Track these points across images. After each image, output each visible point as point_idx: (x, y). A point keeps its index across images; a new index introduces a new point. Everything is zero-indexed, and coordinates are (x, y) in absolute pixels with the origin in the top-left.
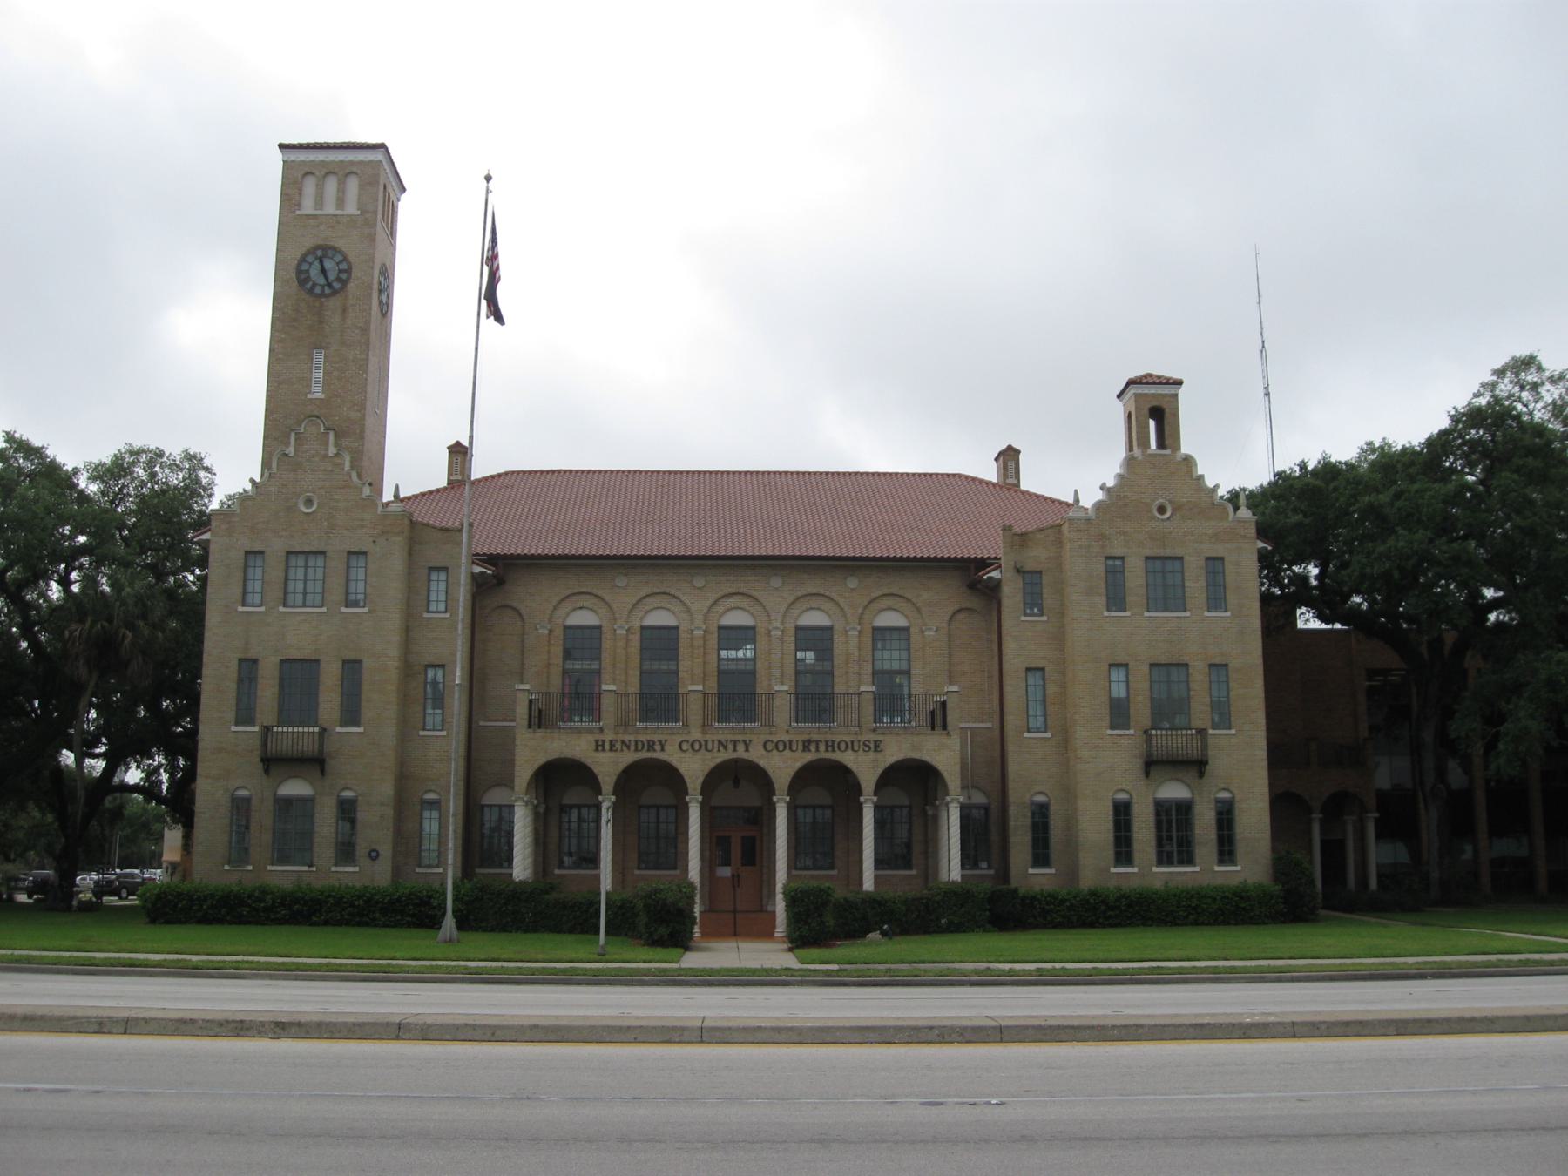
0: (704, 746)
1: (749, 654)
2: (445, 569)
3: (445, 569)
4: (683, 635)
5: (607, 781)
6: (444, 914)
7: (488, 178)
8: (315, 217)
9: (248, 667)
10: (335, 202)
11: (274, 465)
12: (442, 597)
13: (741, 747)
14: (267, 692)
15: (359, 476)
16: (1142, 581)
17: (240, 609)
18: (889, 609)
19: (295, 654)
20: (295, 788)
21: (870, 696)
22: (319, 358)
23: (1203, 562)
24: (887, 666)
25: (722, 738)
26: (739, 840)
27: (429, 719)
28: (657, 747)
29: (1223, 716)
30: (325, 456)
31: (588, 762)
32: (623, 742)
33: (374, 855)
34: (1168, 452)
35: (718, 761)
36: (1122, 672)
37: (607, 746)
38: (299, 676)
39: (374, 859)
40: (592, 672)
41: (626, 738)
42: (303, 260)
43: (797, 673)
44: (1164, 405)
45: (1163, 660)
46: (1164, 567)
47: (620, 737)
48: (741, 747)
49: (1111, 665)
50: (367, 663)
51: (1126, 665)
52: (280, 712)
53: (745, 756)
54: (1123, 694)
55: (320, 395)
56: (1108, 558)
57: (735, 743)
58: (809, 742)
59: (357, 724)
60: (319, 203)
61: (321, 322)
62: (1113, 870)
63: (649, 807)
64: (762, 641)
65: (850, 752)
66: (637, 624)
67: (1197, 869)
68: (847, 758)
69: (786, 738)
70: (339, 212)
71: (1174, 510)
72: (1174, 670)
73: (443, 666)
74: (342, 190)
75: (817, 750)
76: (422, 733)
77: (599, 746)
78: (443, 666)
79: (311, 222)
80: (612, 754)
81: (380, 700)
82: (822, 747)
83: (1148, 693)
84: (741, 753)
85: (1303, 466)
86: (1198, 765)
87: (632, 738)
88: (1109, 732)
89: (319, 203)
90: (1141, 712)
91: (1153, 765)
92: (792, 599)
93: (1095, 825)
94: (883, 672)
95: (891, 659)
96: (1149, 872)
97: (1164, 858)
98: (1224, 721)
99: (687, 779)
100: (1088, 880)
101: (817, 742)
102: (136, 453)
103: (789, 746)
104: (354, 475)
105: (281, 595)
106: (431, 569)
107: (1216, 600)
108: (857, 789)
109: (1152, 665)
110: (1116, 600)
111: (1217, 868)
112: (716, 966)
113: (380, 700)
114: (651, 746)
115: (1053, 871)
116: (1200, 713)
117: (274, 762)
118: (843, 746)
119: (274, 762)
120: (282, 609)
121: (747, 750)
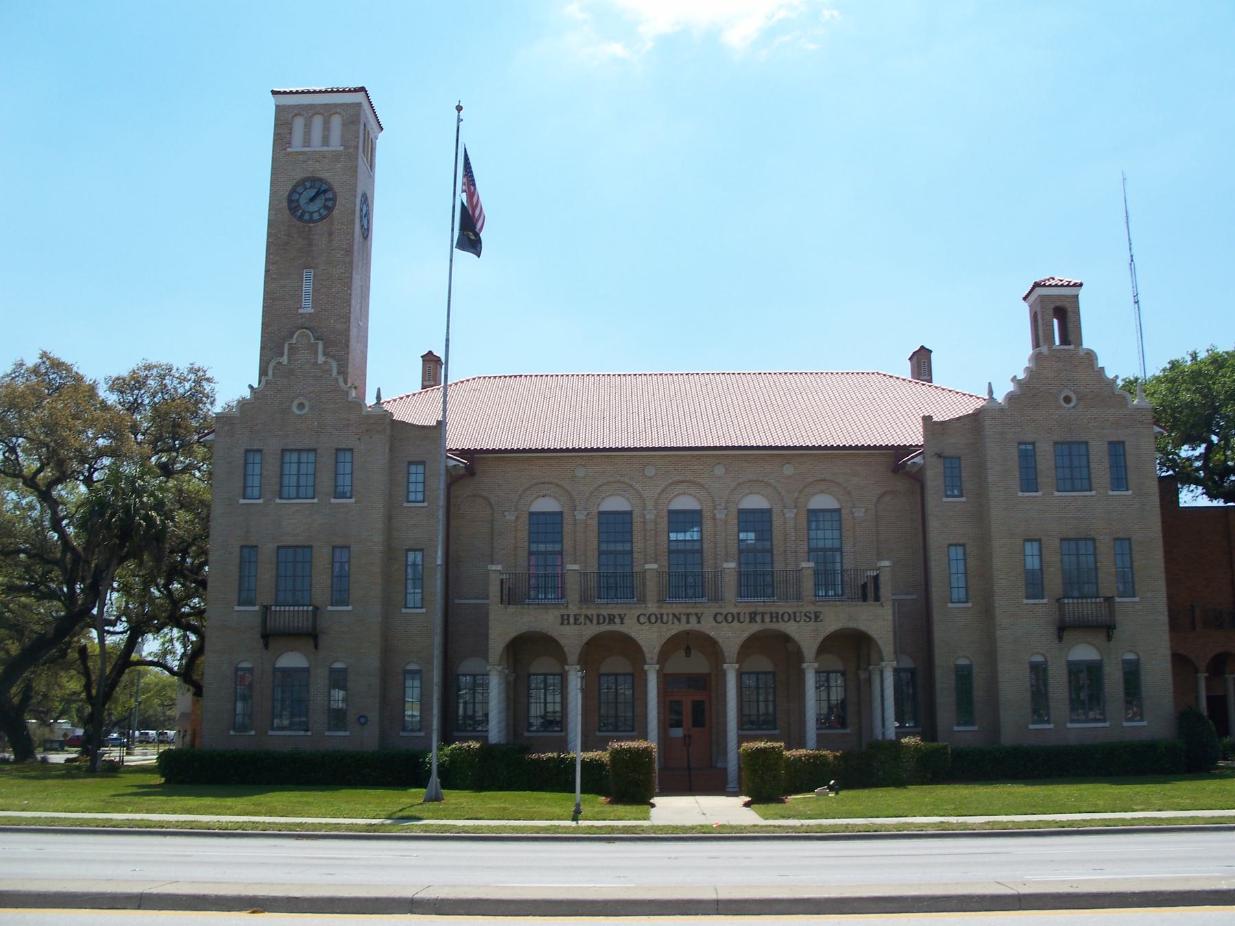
0: (660, 618)
2: (423, 463)
3: (423, 463)
4: (637, 520)
5: (809, 646)
7: (459, 108)
9: (249, 553)
11: (270, 372)
13: (693, 619)
14: (265, 575)
17: (242, 501)
18: (822, 492)
19: (290, 541)
20: (292, 660)
21: (810, 572)
22: (308, 276)
23: (1106, 447)
24: (821, 544)
25: (676, 611)
27: (410, 597)
28: (617, 620)
31: (555, 635)
32: (586, 616)
34: (1072, 347)
35: (674, 632)
36: (1036, 545)
37: (572, 620)
38: (295, 557)
41: (589, 613)
42: (293, 191)
44: (1052, 306)
46: (1072, 453)
47: (584, 612)
48: (693, 619)
51: (1039, 540)
53: (697, 627)
56: (1020, 443)
58: (755, 614)
60: (307, 141)
64: (708, 524)
65: (792, 622)
66: (595, 512)
68: (790, 628)
69: (735, 611)
70: (325, 149)
71: (1078, 399)
72: (1082, 544)
74: (327, 127)
75: (763, 621)
76: (404, 610)
77: (564, 620)
78: (422, 550)
79: (301, 158)
80: (576, 627)
82: (767, 619)
84: (693, 625)
85: (1194, 356)
87: (594, 612)
88: (1026, 601)
89: (307, 141)
90: (1054, 583)
91: (1063, 628)
93: (1013, 684)
95: (825, 537)
99: (645, 649)
100: (1009, 735)
101: (763, 614)
102: (149, 368)
103: (737, 617)
104: (341, 380)
106: (410, 463)
107: (1119, 480)
109: (1061, 540)
110: (1029, 482)
114: (611, 619)
115: (976, 728)
116: (1108, 583)
120: (278, 501)
121: (699, 622)
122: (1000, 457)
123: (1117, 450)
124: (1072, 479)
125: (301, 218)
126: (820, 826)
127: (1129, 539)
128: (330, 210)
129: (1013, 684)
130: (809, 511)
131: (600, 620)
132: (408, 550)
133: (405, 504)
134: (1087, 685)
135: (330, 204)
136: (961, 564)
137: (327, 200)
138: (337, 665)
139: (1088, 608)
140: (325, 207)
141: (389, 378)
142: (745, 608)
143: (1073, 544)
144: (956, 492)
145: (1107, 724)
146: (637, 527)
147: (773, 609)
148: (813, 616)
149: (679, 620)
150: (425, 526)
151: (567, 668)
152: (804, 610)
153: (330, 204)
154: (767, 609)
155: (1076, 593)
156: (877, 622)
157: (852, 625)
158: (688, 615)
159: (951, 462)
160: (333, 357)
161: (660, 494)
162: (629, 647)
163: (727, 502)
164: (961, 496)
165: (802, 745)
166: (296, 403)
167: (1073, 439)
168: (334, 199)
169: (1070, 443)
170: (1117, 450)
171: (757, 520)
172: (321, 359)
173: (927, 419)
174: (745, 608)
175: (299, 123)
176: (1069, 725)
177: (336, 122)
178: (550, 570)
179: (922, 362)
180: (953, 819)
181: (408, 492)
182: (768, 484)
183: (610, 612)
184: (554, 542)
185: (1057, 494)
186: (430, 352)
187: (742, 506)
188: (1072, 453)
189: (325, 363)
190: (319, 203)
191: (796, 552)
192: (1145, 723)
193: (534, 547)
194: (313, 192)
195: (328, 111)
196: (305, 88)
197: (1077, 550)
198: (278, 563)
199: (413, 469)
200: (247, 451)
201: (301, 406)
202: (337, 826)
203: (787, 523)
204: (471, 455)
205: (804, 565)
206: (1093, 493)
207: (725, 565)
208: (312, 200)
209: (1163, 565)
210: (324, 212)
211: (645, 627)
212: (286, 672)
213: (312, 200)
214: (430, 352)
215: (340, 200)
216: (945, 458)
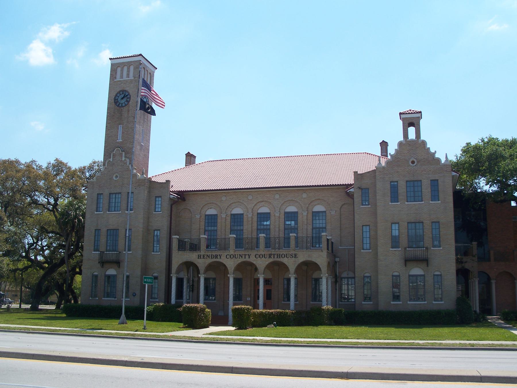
0: (234, 256)
1: (268, 224)
2: (161, 197)
3: (161, 197)
4: (245, 217)
5: (202, 269)
6: (122, 314)
8: (120, 81)
9: (98, 231)
10: (127, 76)
11: (106, 164)
12: (160, 206)
13: (247, 257)
14: (103, 240)
15: (132, 166)
16: (405, 190)
17: (96, 213)
18: (318, 204)
19: (111, 227)
20: (111, 272)
21: (294, 237)
22: (120, 127)
23: (429, 182)
24: (318, 226)
25: (241, 253)
27: (155, 248)
28: (219, 257)
30: (122, 160)
31: (196, 263)
32: (207, 255)
33: (134, 295)
35: (240, 262)
36: (397, 225)
37: (202, 257)
38: (113, 233)
39: (134, 296)
40: (214, 230)
41: (208, 254)
42: (116, 95)
43: (285, 229)
44: (408, 122)
46: (414, 185)
47: (206, 254)
48: (247, 257)
49: (392, 223)
51: (398, 223)
54: (397, 234)
55: (121, 141)
56: (391, 182)
57: (245, 255)
58: (271, 254)
60: (122, 77)
61: (121, 116)
62: (392, 303)
63: (344, 278)
64: (272, 218)
66: (229, 213)
68: (285, 260)
69: (263, 253)
70: (121, 79)
71: (418, 162)
72: (417, 224)
73: (159, 230)
74: (128, 71)
75: (274, 257)
76: (152, 253)
77: (199, 257)
78: (159, 230)
79: (119, 83)
82: (276, 256)
84: (247, 259)
85: (483, 140)
86: (117, 263)
87: (210, 254)
88: (391, 249)
89: (122, 77)
90: (404, 241)
91: (408, 261)
92: (283, 202)
93: (384, 284)
94: (316, 228)
95: (319, 223)
100: (382, 307)
102: (94, 163)
103: (264, 256)
105: (107, 207)
106: (156, 197)
107: (435, 196)
109: (408, 223)
110: (395, 197)
112: (177, 335)
114: (216, 257)
115: (372, 303)
116: (428, 241)
117: (104, 263)
118: (283, 256)
119: (104, 263)
120: (108, 212)
121: (249, 258)
123: (434, 183)
124: (414, 197)
125: (118, 106)
127: (439, 222)
128: (128, 102)
129: (384, 284)
130: (313, 212)
131: (212, 257)
132: (154, 230)
133: (154, 213)
135: (128, 100)
136: (368, 233)
137: (127, 98)
139: (419, 252)
140: (127, 101)
141: (163, 163)
142: (266, 252)
144: (367, 203)
145: (426, 302)
146: (245, 220)
147: (278, 253)
148: (294, 255)
149: (242, 257)
150: (161, 221)
153: (128, 100)
155: (414, 246)
156: (321, 258)
157: (309, 259)
158: (245, 255)
159: (364, 191)
160: (128, 158)
161: (254, 207)
162: (283, 267)
163: (280, 209)
164: (369, 205)
165: (258, 309)
166: (114, 176)
168: (130, 98)
170: (434, 183)
171: (292, 216)
172: (123, 159)
173: (356, 173)
174: (266, 252)
175: (119, 69)
176: (409, 302)
177: (132, 68)
178: (212, 237)
179: (190, 158)
181: (155, 208)
183: (216, 254)
184: (214, 226)
185: (406, 203)
186: (189, 152)
187: (286, 211)
188: (414, 185)
189: (125, 160)
190: (125, 100)
191: (307, 229)
192: (443, 302)
193: (207, 228)
194: (123, 96)
195: (129, 64)
196: (125, 56)
197: (415, 227)
198: (107, 235)
199: (157, 199)
200: (98, 194)
201: (117, 177)
203: (304, 217)
204: (179, 193)
205: (202, 236)
206: (423, 202)
208: (122, 98)
209: (454, 233)
210: (126, 103)
211: (229, 260)
212: (109, 277)
213: (122, 98)
214: (189, 152)
215: (132, 98)
216: (362, 189)
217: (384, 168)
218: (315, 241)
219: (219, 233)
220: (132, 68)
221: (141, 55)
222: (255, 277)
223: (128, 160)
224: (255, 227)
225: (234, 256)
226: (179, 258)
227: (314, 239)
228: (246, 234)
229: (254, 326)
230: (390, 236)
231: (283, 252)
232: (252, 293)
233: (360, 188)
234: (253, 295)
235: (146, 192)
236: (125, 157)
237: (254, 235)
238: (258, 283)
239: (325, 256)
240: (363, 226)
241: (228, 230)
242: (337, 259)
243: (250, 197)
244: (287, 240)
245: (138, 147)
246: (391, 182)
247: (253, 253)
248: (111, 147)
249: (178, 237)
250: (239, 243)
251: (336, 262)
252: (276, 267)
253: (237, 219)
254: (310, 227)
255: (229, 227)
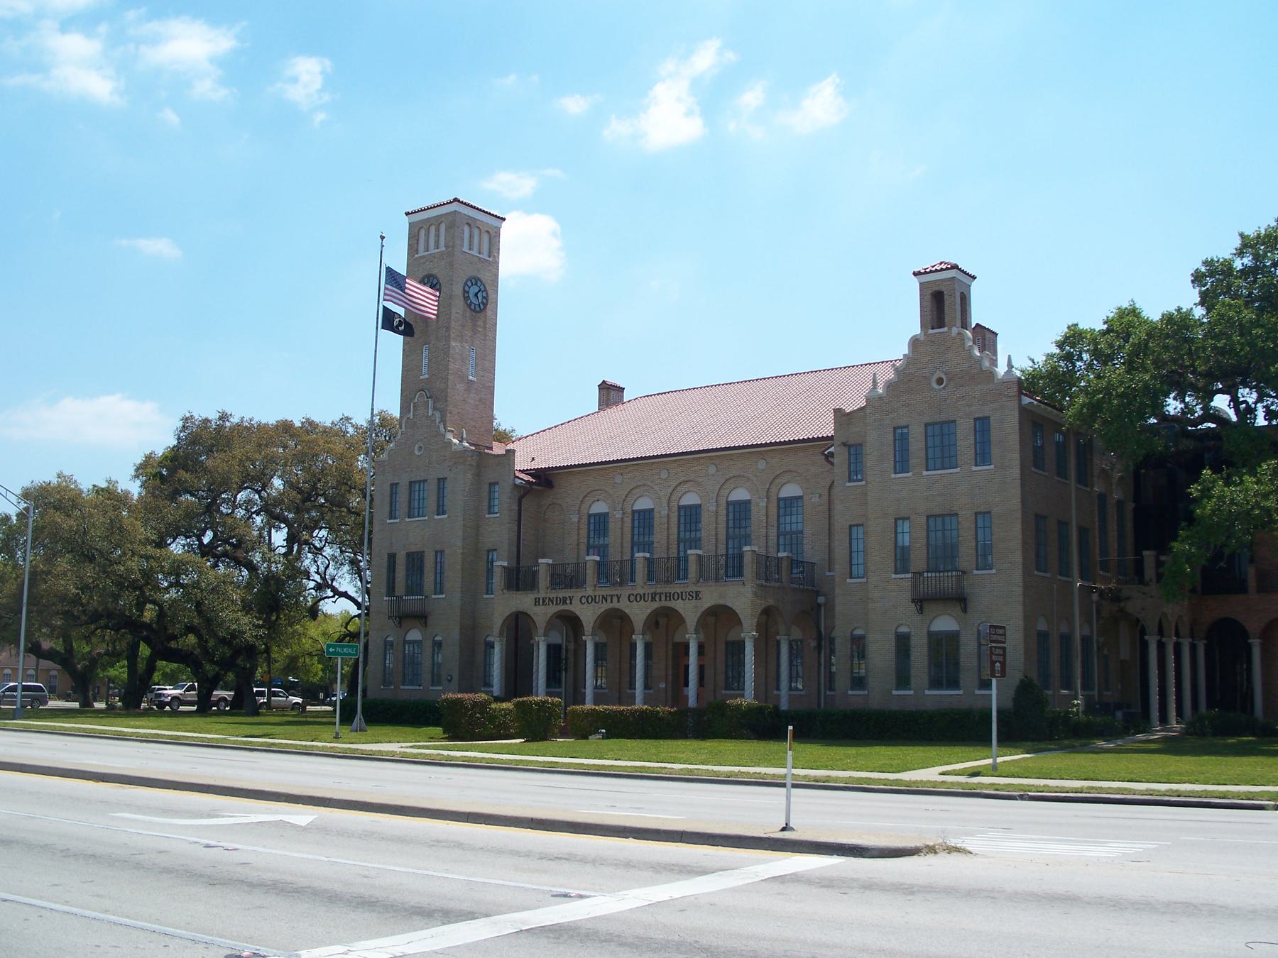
0: (594, 599)
4: (656, 515)
7: (382, 238)
13: (615, 599)
16: (922, 445)
19: (413, 549)
26: (562, 665)
29: (984, 557)
34: (945, 329)
44: (943, 289)
45: (937, 511)
48: (615, 599)
50: (447, 551)
52: (407, 587)
59: (441, 593)
62: (894, 692)
67: (961, 692)
68: (678, 605)
71: (949, 380)
72: (947, 519)
81: (454, 579)
83: (925, 541)
84: (615, 605)
86: (960, 600)
90: (918, 560)
93: (881, 653)
96: (923, 695)
97: (935, 683)
98: (983, 560)
103: (643, 597)
104: (442, 426)
107: (983, 456)
108: (1244, 634)
110: (902, 464)
111: (977, 692)
112: (913, 779)
113: (454, 579)
114: (564, 601)
116: (966, 556)
122: (878, 446)
123: (982, 425)
126: (643, 767)
134: (944, 651)
138: (437, 638)
139: (947, 581)
143: (939, 520)
147: (668, 590)
150: (499, 531)
151: (1146, 637)
152: (688, 590)
154: (664, 590)
156: (742, 598)
157: (721, 602)
162: (623, 618)
167: (944, 419)
169: (942, 423)
170: (982, 425)
173: (838, 412)
175: (422, 233)
177: (443, 227)
179: (610, 394)
180: (736, 769)
182: (748, 479)
185: (925, 473)
187: (783, 494)
191: (767, 536)
195: (438, 220)
202: (79, 729)
204: (537, 473)
207: (588, 558)
217: (881, 398)
218: (732, 567)
219: (611, 550)
220: (443, 227)
221: (456, 200)
222: (678, 639)
223: (438, 415)
224: (674, 537)
225: (594, 599)
226: (502, 605)
227: (730, 561)
228: (614, 554)
229: (564, 734)
230: (891, 547)
231: (676, 588)
232: (670, 672)
233: (844, 444)
234: (670, 678)
235: (469, 476)
236: (435, 409)
237: (627, 557)
238: (687, 654)
239: (750, 595)
240: (851, 527)
241: (583, 547)
242: (821, 600)
243: (664, 475)
244: (682, 561)
245: (461, 387)
246: (895, 429)
247: (625, 591)
248: (416, 388)
249: (598, 558)
250: (603, 570)
251: (819, 606)
252: (664, 620)
253: (644, 519)
254: (773, 532)
255: (628, 538)
